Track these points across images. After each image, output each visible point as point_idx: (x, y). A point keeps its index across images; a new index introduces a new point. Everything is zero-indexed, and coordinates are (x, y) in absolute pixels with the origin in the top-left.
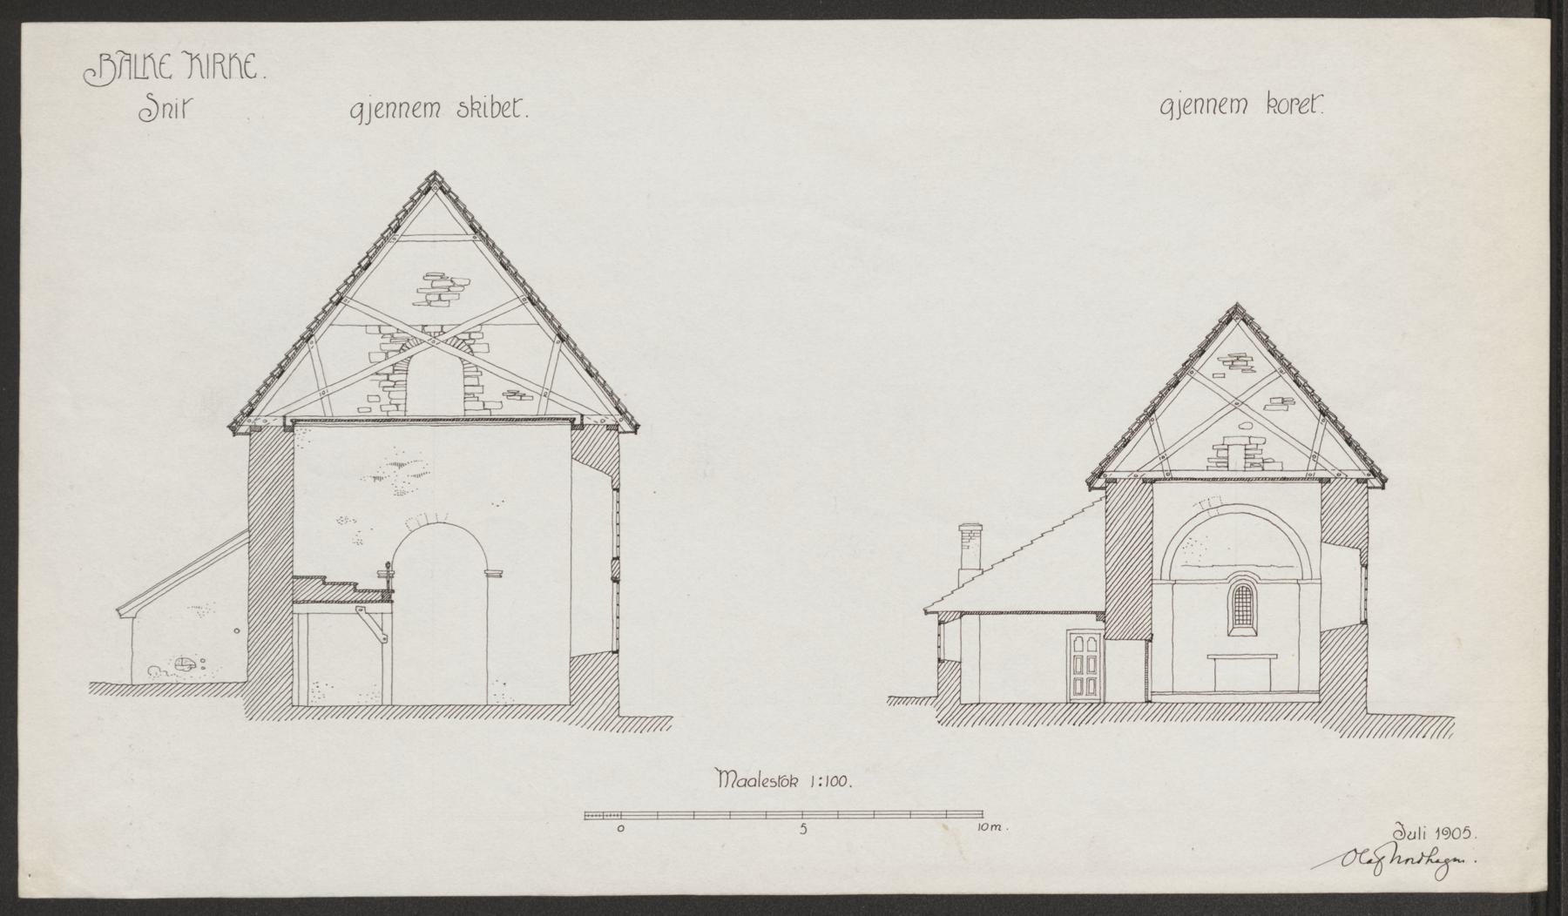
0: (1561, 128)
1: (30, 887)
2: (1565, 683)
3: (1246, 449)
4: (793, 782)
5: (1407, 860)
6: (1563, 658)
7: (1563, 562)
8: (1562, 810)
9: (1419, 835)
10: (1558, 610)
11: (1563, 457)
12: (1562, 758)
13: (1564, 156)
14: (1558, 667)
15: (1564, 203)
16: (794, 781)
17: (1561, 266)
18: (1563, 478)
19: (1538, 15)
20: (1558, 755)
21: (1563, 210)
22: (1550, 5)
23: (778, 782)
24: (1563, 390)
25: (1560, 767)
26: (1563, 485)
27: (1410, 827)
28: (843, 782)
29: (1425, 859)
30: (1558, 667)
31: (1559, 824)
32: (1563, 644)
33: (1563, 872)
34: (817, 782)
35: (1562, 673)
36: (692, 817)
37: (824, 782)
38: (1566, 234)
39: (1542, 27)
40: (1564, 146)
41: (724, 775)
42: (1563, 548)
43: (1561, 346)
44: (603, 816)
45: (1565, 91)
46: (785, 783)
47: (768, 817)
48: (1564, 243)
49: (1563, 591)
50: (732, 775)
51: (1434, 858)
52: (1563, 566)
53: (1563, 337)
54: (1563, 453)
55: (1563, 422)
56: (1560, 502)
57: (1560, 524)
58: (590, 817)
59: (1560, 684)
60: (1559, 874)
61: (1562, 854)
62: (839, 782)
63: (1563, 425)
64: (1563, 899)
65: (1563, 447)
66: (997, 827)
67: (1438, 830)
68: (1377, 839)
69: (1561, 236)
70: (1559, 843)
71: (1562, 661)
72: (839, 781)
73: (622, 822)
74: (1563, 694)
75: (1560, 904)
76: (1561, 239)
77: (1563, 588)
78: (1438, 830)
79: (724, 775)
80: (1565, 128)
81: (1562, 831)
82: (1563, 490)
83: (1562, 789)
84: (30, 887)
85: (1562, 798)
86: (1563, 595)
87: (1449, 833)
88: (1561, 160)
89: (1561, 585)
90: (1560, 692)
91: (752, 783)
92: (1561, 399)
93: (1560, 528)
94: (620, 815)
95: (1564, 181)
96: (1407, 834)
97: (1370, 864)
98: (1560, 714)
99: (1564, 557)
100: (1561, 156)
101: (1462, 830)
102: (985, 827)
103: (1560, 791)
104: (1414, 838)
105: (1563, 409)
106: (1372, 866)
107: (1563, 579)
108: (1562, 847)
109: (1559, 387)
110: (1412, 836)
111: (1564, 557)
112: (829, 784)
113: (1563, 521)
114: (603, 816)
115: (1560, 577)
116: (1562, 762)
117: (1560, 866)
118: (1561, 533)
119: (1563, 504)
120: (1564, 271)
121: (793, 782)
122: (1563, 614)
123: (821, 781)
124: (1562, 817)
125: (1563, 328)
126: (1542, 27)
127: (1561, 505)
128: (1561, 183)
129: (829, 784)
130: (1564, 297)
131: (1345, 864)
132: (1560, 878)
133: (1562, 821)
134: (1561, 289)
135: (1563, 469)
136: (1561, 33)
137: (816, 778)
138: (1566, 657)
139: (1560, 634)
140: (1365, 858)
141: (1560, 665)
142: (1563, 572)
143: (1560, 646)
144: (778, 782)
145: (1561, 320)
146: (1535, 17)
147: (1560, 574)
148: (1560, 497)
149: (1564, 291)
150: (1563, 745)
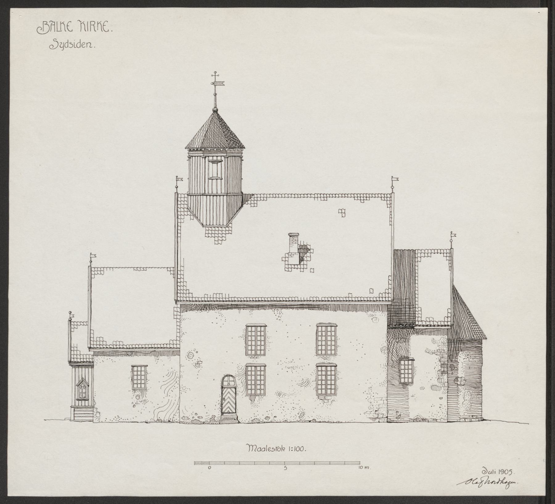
1: (13, 491)
2: (553, 405)
4: (283, 449)
5: (492, 483)
6: (552, 395)
7: (552, 354)
9: (493, 472)
10: (551, 209)
11: (552, 310)
12: (552, 436)
13: (553, 184)
14: (550, 398)
15: (552, 204)
18: (552, 319)
19: (542, 6)
20: (551, 50)
21: (552, 207)
22: (547, 1)
24: (552, 282)
26: (552, 322)
27: (489, 469)
28: (302, 449)
29: (500, 482)
30: (550, 398)
32: (552, 388)
33: (552, 484)
34: (291, 449)
35: (552, 401)
36: (239, 464)
37: (293, 449)
40: (553, 181)
41: (251, 447)
42: (552, 348)
43: (551, 264)
44: (202, 463)
45: (553, 158)
47: (300, 464)
48: (553, 221)
49: (552, 366)
50: (254, 447)
51: (504, 481)
52: (552, 356)
53: (552, 260)
54: (552, 309)
56: (551, 329)
57: (551, 338)
58: (200, 462)
59: (551, 405)
60: (551, 484)
61: (552, 476)
62: (300, 449)
64: (552, 495)
65: (552, 306)
68: (477, 474)
69: (551, 218)
70: (550, 472)
71: (552, 396)
74: (552, 409)
79: (251, 447)
81: (552, 467)
82: (552, 324)
83: (552, 449)
84: (13, 491)
85: (552, 452)
87: (503, 472)
88: (551, 186)
89: (551, 364)
90: (551, 409)
91: (263, 450)
93: (551, 340)
94: (209, 463)
95: (552, 195)
97: (477, 484)
101: (509, 470)
102: (361, 467)
103: (551, 450)
104: (491, 473)
105: (552, 290)
106: (478, 485)
107: (552, 361)
108: (552, 473)
109: (550, 311)
111: (552, 352)
112: (296, 450)
114: (202, 463)
115: (551, 360)
117: (551, 481)
118: (551, 342)
119: (552, 330)
120: (552, 233)
121: (283, 449)
122: (552, 376)
123: (292, 449)
124: (552, 461)
127: (551, 331)
129: (296, 450)
130: (552, 243)
131: (473, 483)
132: (551, 486)
133: (552, 462)
134: (551, 240)
135: (552, 315)
136: (552, 133)
137: (291, 448)
139: (551, 385)
140: (475, 482)
141: (551, 397)
142: (552, 358)
143: (551, 389)
145: (551, 253)
147: (551, 359)
149: (553, 241)
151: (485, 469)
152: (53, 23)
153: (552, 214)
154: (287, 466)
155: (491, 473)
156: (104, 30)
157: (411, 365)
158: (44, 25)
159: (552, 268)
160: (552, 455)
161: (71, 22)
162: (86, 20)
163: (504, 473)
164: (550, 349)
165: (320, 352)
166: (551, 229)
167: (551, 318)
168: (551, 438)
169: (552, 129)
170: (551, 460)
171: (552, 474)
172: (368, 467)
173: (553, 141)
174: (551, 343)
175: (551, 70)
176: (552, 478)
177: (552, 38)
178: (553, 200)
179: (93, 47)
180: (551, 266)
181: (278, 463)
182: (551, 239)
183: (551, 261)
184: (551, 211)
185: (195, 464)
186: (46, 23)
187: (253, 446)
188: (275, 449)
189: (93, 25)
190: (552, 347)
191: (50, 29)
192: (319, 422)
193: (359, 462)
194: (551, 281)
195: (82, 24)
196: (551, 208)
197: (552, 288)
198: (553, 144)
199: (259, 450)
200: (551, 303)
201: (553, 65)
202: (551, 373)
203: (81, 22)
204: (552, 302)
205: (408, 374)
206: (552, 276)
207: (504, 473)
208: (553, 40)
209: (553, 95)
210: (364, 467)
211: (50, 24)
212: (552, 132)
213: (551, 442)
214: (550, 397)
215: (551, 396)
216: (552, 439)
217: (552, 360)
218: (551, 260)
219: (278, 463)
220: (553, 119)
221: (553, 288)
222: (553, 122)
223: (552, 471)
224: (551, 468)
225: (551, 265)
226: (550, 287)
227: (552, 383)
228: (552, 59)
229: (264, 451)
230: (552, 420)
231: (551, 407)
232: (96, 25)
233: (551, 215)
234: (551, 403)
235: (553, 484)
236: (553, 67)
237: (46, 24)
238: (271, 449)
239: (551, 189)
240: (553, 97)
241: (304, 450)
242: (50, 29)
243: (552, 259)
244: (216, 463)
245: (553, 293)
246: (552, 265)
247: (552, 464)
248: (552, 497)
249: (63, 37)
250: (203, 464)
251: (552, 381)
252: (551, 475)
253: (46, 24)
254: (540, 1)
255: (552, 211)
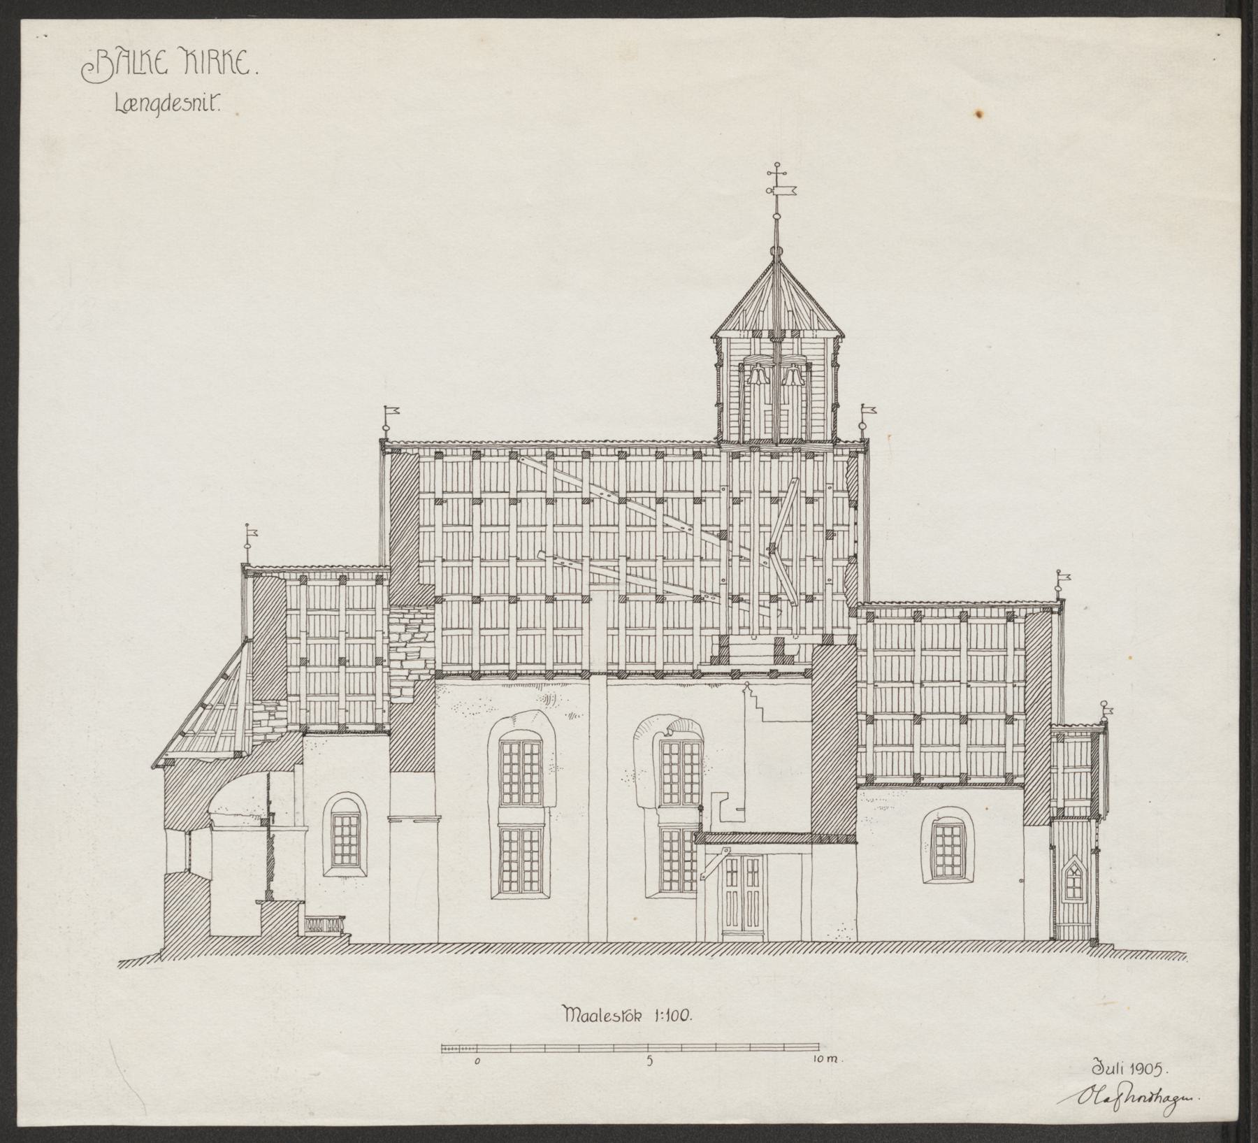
0: (1251, 351)
3: (784, 404)
4: (637, 1017)
6: (1252, 853)
8: (1252, 996)
9: (1116, 1069)
10: (1249, 432)
11: (1252, 662)
12: (1252, 947)
13: (1253, 376)
15: (1253, 421)
16: (638, 1016)
17: (1251, 481)
18: (1253, 682)
19: (1228, 14)
20: (1247, 945)
21: (1253, 427)
23: (624, 1017)
24: (1253, 599)
25: (1249, 956)
26: (1253, 688)
31: (1249, 1010)
35: (1252, 867)
38: (1255, 451)
39: (1232, 27)
41: (570, 1010)
42: (1252, 748)
43: (1250, 557)
44: (460, 1049)
46: (629, 1017)
48: (1253, 459)
49: (1252, 789)
50: (577, 1011)
52: (1252, 765)
53: (1253, 548)
54: (1252, 658)
55: (1252, 629)
56: (1250, 705)
57: (1250, 726)
58: (464, 1050)
61: (1252, 1038)
63: (1253, 632)
65: (1253, 652)
66: (834, 1059)
67: (1133, 1066)
69: (1250, 452)
70: (1248, 1029)
71: (1252, 856)
72: (682, 1016)
73: (478, 1055)
74: (1252, 887)
75: (1250, 1085)
76: (1251, 456)
77: (1252, 786)
78: (1133, 1066)
79: (570, 1010)
80: (1254, 350)
81: (1252, 1017)
82: (1252, 693)
83: (1252, 977)
84: (26, 1118)
85: (1251, 985)
86: (1252, 793)
88: (1251, 380)
89: (1250, 784)
92: (1250, 607)
93: (1250, 730)
94: (476, 1048)
95: (1253, 401)
96: (1106, 1069)
98: (1249, 907)
99: (1253, 757)
100: (1250, 376)
101: (1154, 1066)
104: (1113, 1072)
105: (1252, 616)
110: (1110, 1071)
113: (1252, 723)
114: (460, 1049)
115: (1249, 776)
116: (1252, 951)
118: (1250, 733)
119: (1252, 706)
121: (637, 1017)
122: (1252, 811)
124: (1251, 1003)
125: (1253, 539)
126: (1232, 27)
127: (1250, 708)
128: (1251, 401)
129: (625, 1020)
132: (1249, 1061)
133: (1252, 1007)
135: (1252, 673)
136: (1251, 260)
137: (659, 1013)
138: (1255, 851)
139: (1249, 830)
143: (1249, 841)
144: (624, 1017)
145: (1250, 531)
146: (1226, 16)
148: (1250, 701)
150: (1253, 934)
151: (1099, 1063)
152: (124, 51)
153: (1253, 444)
154: (654, 1056)
155: (1113, 1072)
156: (240, 70)
157: (538, 764)
158: (101, 59)
159: (1252, 566)
160: (1251, 991)
161: (164, 51)
162: (199, 47)
163: (1144, 1072)
164: (1247, 749)
165: (956, 831)
166: (1250, 478)
167: (1250, 679)
168: (1249, 951)
169: (1251, 250)
170: (1249, 1003)
171: (1251, 1033)
172: (834, 1059)
173: (1253, 278)
174: (1250, 736)
175: (1251, 115)
176: (1252, 1042)
177: (1252, 45)
178: (1253, 411)
179: (216, 110)
180: (1250, 561)
181: (628, 1048)
182: (1250, 499)
183: (1250, 550)
184: (1251, 437)
185: (444, 1051)
186: (104, 54)
187: (573, 1010)
188: (621, 1017)
189: (216, 58)
190: (1252, 745)
191: (115, 70)
192: (112, 1049)
193: (817, 1045)
194: (1250, 596)
195: (191, 57)
196: (1250, 431)
197: (1253, 611)
198: (1253, 283)
199: (585, 1019)
200: (1250, 646)
201: (1255, 219)
202: (1249, 805)
203: (187, 51)
204: (1252, 644)
205: (953, 845)
206: (1253, 585)
207: (1144, 1072)
208: (1254, 49)
209: (1254, 173)
210: (826, 1059)
211: (114, 57)
212: (1252, 257)
213: (1250, 961)
214: (1247, 857)
215: (1250, 856)
216: (1252, 954)
217: (1252, 774)
218: (1250, 546)
219: (628, 1048)
220: (1254, 228)
221: (1255, 612)
222: (1254, 234)
223: (1251, 1027)
224: (1249, 1019)
225: (1249, 559)
226: (1249, 609)
227: (1252, 826)
228: (1252, 90)
229: (596, 1020)
230: (1253, 910)
231: (1249, 882)
232: (220, 58)
233: (1250, 445)
234: (1249, 872)
235: (1254, 1056)
236: (1254, 110)
237: (105, 57)
238: (612, 1016)
239: (1251, 387)
240: (1254, 179)
241: (689, 1018)
242: (115, 70)
243: (1253, 545)
244: (495, 1049)
245: (1254, 624)
246: (1253, 559)
247: (1252, 1012)
248: (1252, 1086)
249: (151, 87)
250: (461, 1051)
251: (1252, 824)
252: (1249, 1035)
253: (105, 57)
254: (1224, 1)
255: (1253, 436)
